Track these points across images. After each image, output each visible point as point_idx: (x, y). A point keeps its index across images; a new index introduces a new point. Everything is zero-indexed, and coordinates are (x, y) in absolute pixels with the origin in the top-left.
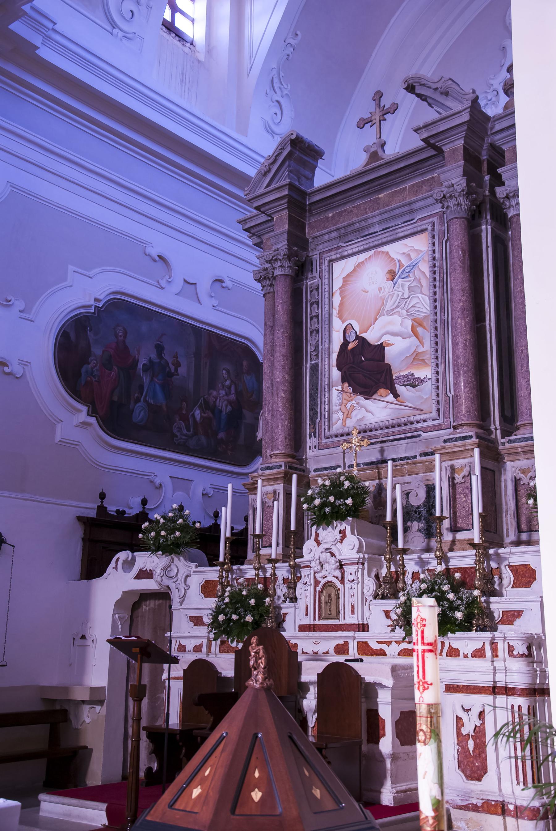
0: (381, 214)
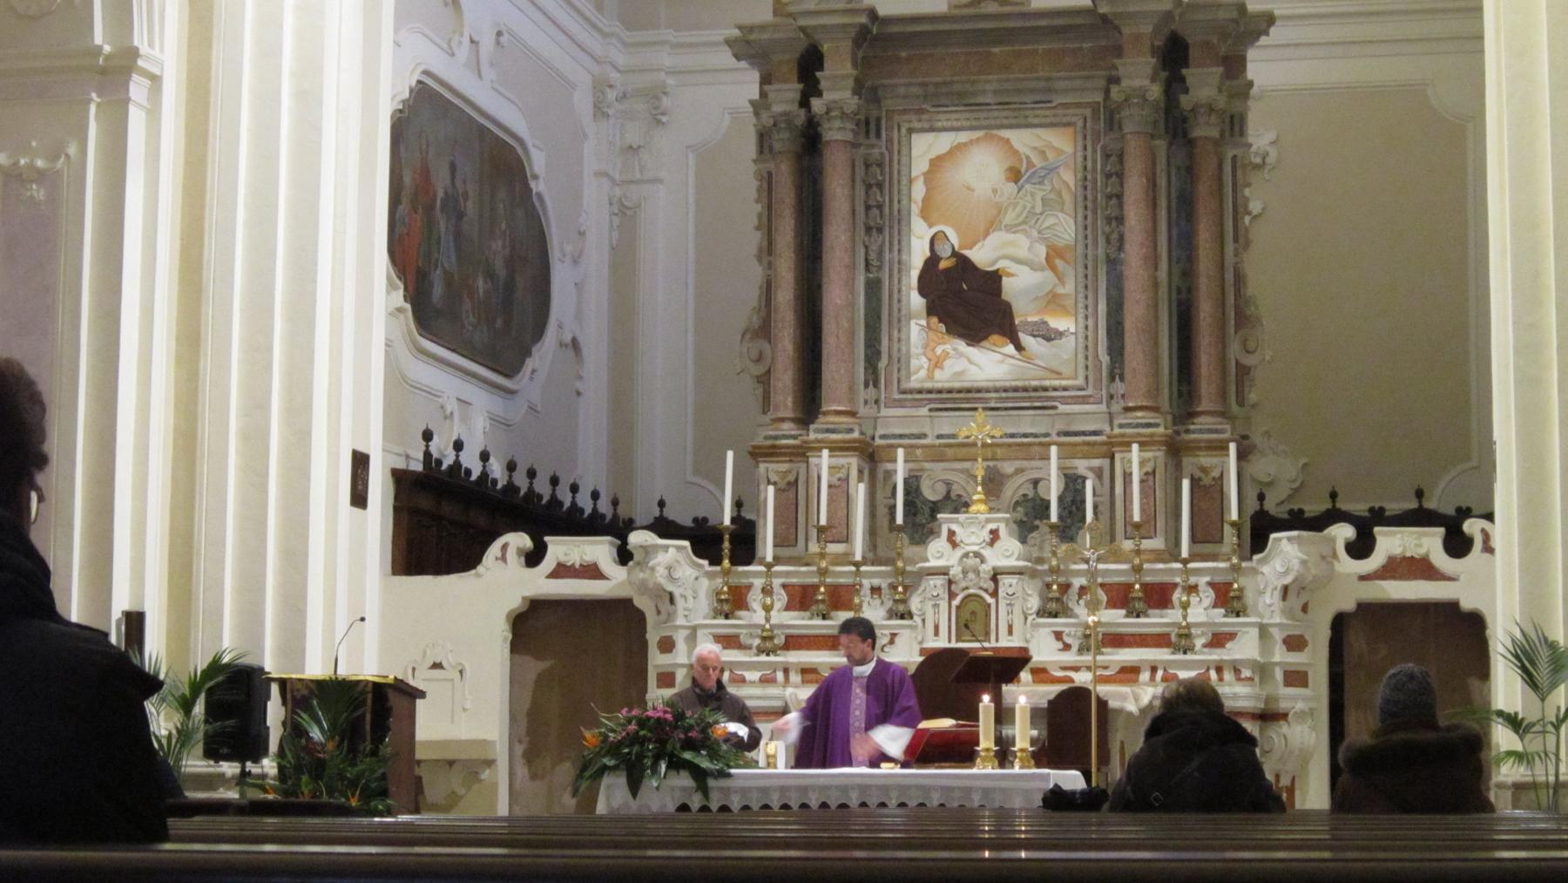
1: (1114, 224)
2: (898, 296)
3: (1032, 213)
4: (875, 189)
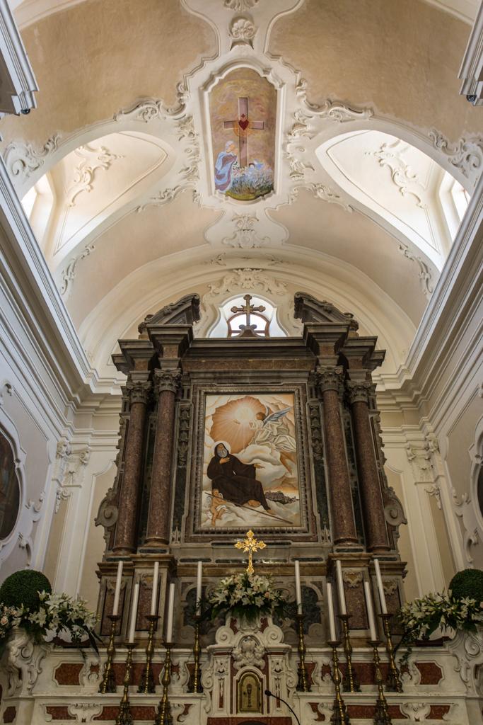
1: (317, 442)
2: (198, 479)
3: (272, 435)
4: (184, 433)
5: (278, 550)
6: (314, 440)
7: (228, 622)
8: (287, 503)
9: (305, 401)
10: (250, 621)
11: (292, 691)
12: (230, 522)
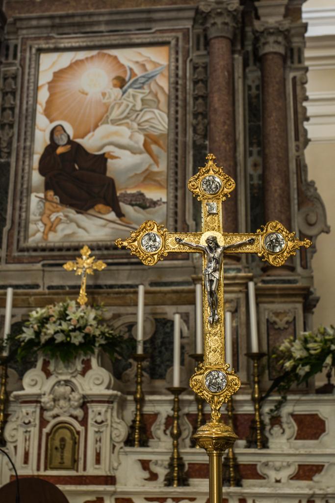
0: (111, 14)
1: (200, 118)
3: (133, 110)
5: (133, 272)
6: (196, 115)
7: (40, 364)
8: (150, 207)
9: (187, 54)
10: (68, 361)
11: (118, 446)
12: (68, 236)
